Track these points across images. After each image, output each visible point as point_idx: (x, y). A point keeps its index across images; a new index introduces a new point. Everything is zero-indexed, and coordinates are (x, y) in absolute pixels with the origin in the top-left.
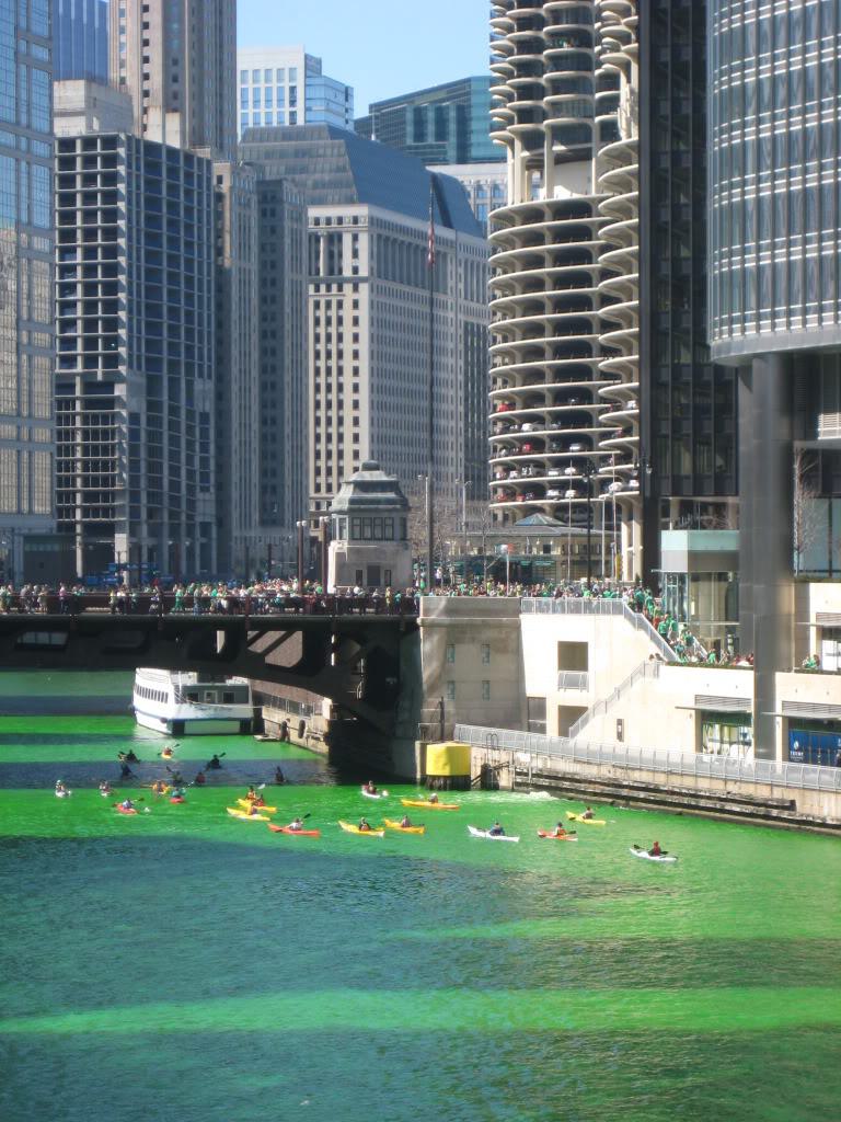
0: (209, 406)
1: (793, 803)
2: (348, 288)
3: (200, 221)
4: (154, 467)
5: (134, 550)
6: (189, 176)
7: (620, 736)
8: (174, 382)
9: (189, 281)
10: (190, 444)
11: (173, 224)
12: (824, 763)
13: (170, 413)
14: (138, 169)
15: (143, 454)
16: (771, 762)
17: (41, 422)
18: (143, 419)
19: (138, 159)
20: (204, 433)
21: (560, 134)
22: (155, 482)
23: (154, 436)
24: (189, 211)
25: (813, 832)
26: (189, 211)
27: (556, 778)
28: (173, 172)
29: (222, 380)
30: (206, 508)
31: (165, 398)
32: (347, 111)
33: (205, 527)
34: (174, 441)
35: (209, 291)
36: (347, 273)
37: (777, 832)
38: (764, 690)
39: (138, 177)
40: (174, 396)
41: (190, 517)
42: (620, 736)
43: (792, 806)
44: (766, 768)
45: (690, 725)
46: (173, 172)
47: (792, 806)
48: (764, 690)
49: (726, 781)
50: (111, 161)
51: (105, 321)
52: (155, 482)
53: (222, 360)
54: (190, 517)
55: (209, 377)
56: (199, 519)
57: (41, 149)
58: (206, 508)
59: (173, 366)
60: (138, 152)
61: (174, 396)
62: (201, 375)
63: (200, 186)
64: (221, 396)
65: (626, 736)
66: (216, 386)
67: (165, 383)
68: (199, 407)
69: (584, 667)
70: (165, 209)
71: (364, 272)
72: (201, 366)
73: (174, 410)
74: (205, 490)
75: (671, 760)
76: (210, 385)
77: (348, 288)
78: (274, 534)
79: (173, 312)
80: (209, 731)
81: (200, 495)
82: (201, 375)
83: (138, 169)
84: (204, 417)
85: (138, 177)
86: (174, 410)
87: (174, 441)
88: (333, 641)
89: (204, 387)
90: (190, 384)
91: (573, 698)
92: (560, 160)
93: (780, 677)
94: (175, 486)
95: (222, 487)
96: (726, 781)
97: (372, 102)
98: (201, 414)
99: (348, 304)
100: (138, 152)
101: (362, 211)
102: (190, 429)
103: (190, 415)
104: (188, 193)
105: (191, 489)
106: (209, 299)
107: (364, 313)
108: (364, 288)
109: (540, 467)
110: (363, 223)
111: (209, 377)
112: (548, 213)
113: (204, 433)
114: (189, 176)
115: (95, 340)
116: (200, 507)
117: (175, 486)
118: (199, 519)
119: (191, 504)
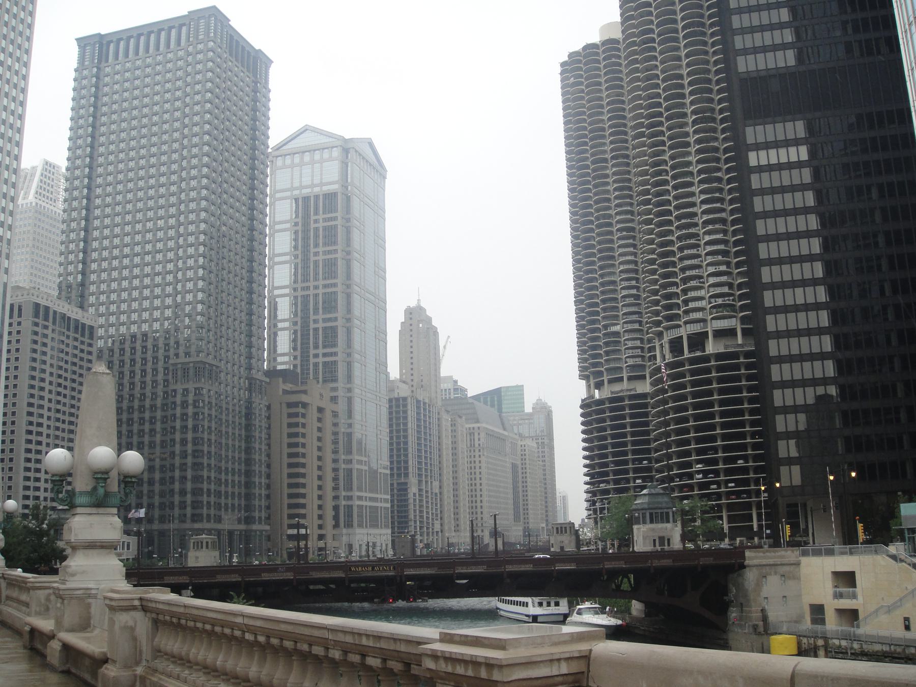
0: (437, 491)
5: (270, 201)
7: (907, 628)
11: (425, 427)
15: (418, 507)
18: (417, 495)
23: (421, 501)
30: (437, 527)
33: (437, 532)
41: (433, 529)
42: (907, 628)
49: (890, 645)
51: (404, 442)
54: (433, 529)
56: (435, 530)
58: (437, 527)
65: (912, 626)
73: (427, 492)
74: (437, 520)
80: (301, 136)
81: (435, 521)
84: (436, 494)
88: (332, 586)
89: (436, 484)
90: (431, 482)
94: (427, 518)
96: (890, 645)
97: (561, 61)
103: (432, 493)
105: (433, 519)
115: (400, 461)
116: (435, 525)
117: (427, 518)
118: (435, 530)
119: (433, 524)
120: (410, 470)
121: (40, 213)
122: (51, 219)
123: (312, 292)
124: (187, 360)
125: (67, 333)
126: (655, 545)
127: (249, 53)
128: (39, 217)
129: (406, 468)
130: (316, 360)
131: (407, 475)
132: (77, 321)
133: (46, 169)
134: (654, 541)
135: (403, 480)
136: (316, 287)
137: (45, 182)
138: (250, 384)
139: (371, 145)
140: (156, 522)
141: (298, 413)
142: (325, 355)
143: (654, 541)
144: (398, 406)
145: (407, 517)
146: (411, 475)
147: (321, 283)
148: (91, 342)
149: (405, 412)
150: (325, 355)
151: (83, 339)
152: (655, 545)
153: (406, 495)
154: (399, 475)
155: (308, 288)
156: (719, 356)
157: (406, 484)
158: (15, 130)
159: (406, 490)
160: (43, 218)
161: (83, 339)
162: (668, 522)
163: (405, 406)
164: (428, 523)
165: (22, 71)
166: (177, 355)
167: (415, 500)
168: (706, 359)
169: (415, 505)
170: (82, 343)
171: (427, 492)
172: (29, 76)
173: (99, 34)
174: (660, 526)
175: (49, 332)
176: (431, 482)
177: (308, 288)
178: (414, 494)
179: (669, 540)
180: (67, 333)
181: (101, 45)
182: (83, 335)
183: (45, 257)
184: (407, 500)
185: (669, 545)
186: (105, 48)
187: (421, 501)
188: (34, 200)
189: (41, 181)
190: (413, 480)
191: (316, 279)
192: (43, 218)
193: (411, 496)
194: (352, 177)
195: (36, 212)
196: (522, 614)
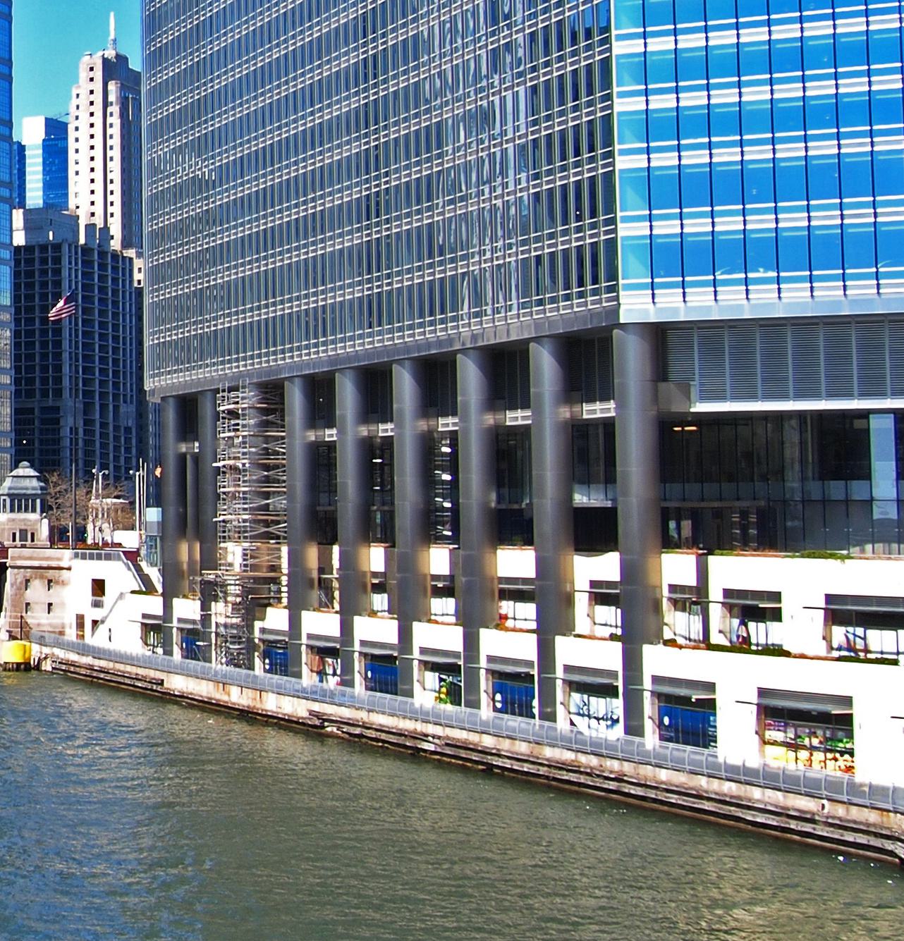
1: (163, 681)
3: (123, 298)
6: (115, 269)
8: (103, 407)
9: (116, 339)
10: (116, 448)
12: (521, 715)
13: (114, 430)
14: (76, 264)
16: (409, 700)
19: (76, 259)
20: (128, 440)
24: (115, 292)
25: (536, 783)
26: (115, 292)
27: (401, 735)
28: (102, 267)
31: (97, 416)
34: (104, 446)
35: (131, 344)
37: (151, 700)
38: (347, 628)
39: (76, 270)
43: (161, 683)
44: (298, 683)
45: (137, 630)
46: (102, 267)
47: (161, 683)
48: (347, 628)
55: (131, 402)
60: (76, 253)
62: (125, 402)
63: (124, 275)
66: (137, 410)
67: (111, 407)
68: (123, 423)
69: (103, 594)
70: (96, 291)
72: (125, 396)
73: (104, 425)
79: (103, 360)
82: (125, 402)
83: (76, 264)
84: (128, 430)
85: (76, 270)
86: (104, 425)
90: (116, 408)
91: (97, 614)
93: (305, 614)
98: (125, 428)
100: (76, 253)
102: (116, 438)
103: (116, 428)
104: (115, 280)
106: (131, 350)
111: (131, 402)
113: (128, 440)
114: (115, 269)
126: (14, 540)
129: (58, 380)
131: (58, 393)
134: (14, 535)
135: (50, 403)
143: (14, 535)
144: (30, 262)
149: (58, 272)
152: (14, 540)
154: (45, 394)
157: (57, 409)
159: (57, 421)
162: (34, 510)
163: (58, 260)
174: (23, 516)
176: (116, 408)
179: (33, 535)
184: (57, 441)
185: (33, 540)
190: (70, 405)
193: (66, 432)
196: (443, 623)
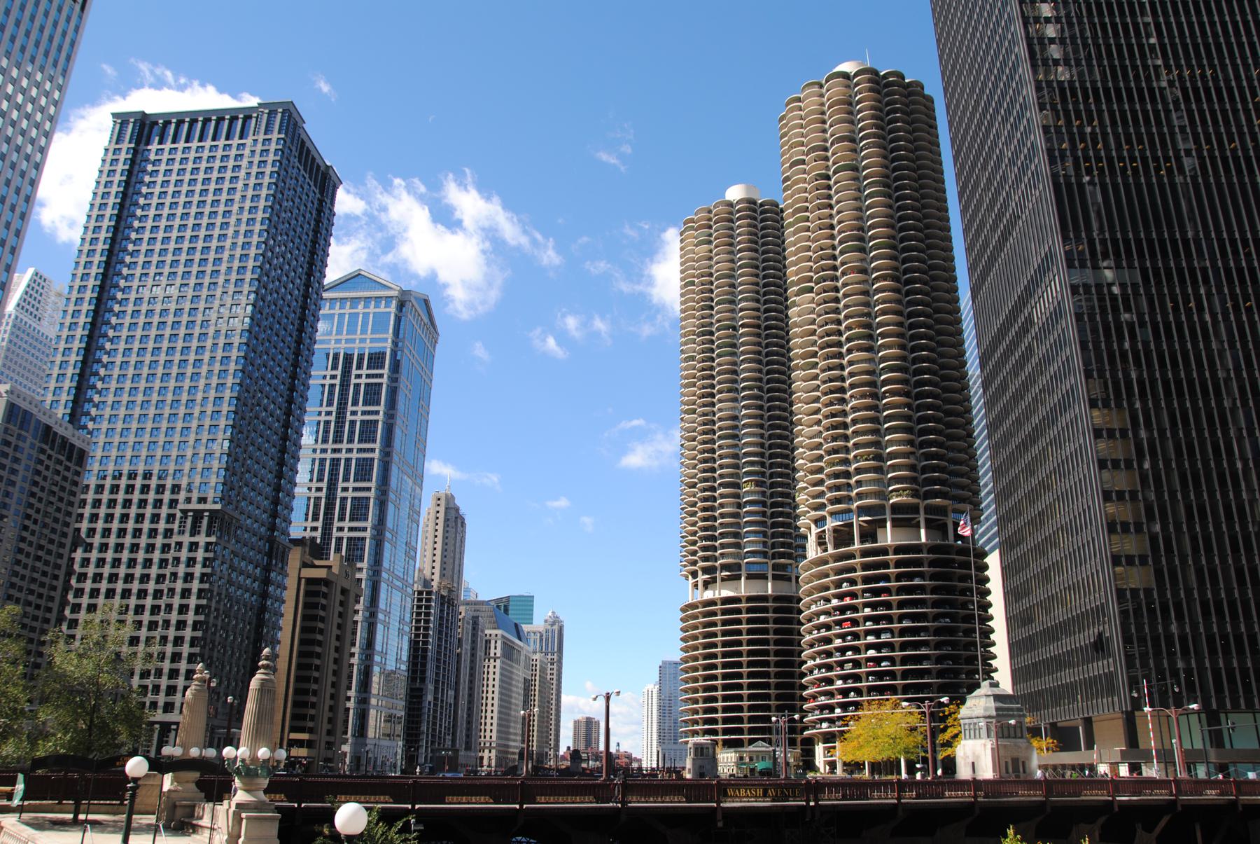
0: (452, 702)
2: (492, 661)
4: (434, 724)
8: (443, 690)
17: (374, 707)
21: (725, 567)
22: (434, 730)
23: (435, 711)
29: (457, 691)
32: (972, 470)
34: (441, 713)
36: (492, 655)
40: (442, 696)
50: (428, 600)
52: (434, 730)
53: (457, 683)
57: (409, 590)
59: (443, 683)
61: (442, 696)
64: (456, 697)
71: (498, 655)
73: (442, 701)
75: (1251, 715)
76: (453, 693)
77: (492, 661)
78: (469, 753)
87: (441, 713)
89: (451, 693)
92: (723, 580)
94: (440, 732)
95: (454, 734)
99: (492, 666)
101: (499, 632)
107: (498, 670)
108: (498, 661)
109: (829, 667)
110: (499, 637)
112: (719, 602)
117: (440, 732)
120: (428, 674)
121: (19, 329)
122: (33, 337)
123: (343, 455)
124: (201, 507)
125: (49, 452)
127: (318, 167)
128: (18, 332)
129: (423, 672)
130: (340, 534)
131: (423, 680)
132: (63, 437)
133: (35, 281)
135: (418, 685)
136: (350, 450)
137: (31, 296)
138: (271, 548)
139: (426, 302)
140: (160, 711)
141: (319, 592)
142: (351, 529)
145: (418, 728)
146: (427, 681)
147: (343, 455)
148: (78, 469)
150: (351, 529)
151: (68, 464)
153: (420, 703)
155: (339, 451)
156: (898, 550)
157: (421, 690)
158: (32, 164)
159: (421, 697)
160: (22, 335)
161: (68, 464)
164: (440, 738)
165: (21, 165)
166: (188, 500)
167: (429, 709)
168: (884, 551)
169: (429, 716)
170: (67, 469)
171: (442, 701)
172: (62, 103)
173: (143, 112)
175: (146, 294)
177: (339, 451)
178: (430, 703)
180: (49, 452)
181: (143, 125)
182: (69, 459)
183: (31, 362)
184: (420, 709)
186: (146, 129)
187: (435, 711)
188: (14, 312)
189: (27, 293)
191: (351, 441)
192: (22, 335)
194: (404, 334)
195: (14, 326)
